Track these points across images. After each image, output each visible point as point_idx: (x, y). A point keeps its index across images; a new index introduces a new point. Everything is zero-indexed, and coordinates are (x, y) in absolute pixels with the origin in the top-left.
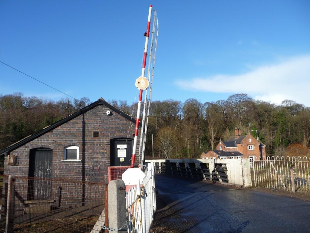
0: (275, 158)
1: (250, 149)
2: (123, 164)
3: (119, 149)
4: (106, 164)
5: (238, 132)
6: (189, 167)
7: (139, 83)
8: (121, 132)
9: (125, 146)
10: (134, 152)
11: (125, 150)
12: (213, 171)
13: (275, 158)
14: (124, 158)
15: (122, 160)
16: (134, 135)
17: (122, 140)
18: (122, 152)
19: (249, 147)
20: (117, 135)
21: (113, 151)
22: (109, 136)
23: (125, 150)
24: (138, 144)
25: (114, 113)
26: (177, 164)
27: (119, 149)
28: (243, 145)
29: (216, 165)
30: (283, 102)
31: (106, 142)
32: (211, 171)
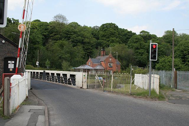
0: (126, 74)
2: (11, 72)
3: (9, 63)
4: (1, 72)
5: (103, 53)
6: (63, 77)
7: (20, 27)
8: (11, 54)
9: (13, 62)
10: (17, 66)
11: (172, 30)
12: (69, 79)
13: (126, 74)
14: (13, 69)
15: (11, 70)
16: (17, 57)
17: (12, 59)
18: (11, 66)
19: (109, 64)
20: (8, 55)
21: (6, 65)
22: (3, 56)
23: (13, 64)
24: (19, 61)
25: (7, 42)
26: (50, 74)
27: (9, 63)
29: (71, 75)
30: (141, 32)
31: (2, 59)
32: (68, 78)
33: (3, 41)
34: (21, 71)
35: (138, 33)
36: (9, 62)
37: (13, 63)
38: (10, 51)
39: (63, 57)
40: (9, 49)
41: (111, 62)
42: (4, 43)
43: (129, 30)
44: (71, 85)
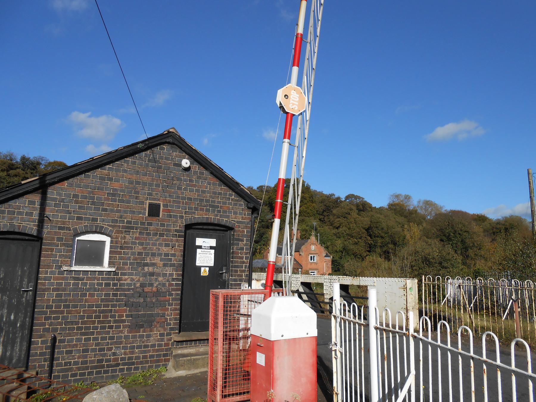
1: (311, 260)
3: (200, 247)
14: (210, 267)
19: (311, 257)
20: (199, 216)
22: (182, 217)
23: (213, 251)
25: (196, 167)
28: (303, 253)
31: (176, 231)
33: (186, 163)
34: (242, 276)
35: (343, 198)
36: (199, 241)
37: (211, 248)
38: (207, 201)
39: (446, 239)
40: (204, 192)
41: (315, 252)
42: (187, 169)
43: (327, 192)
44: (324, 313)
